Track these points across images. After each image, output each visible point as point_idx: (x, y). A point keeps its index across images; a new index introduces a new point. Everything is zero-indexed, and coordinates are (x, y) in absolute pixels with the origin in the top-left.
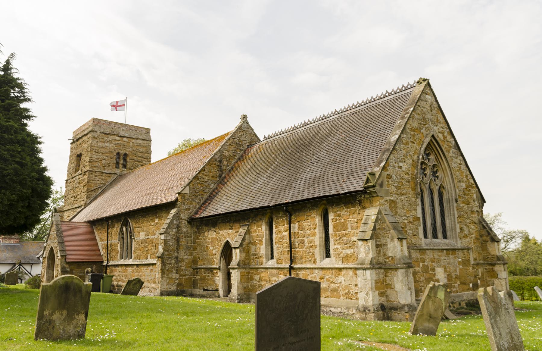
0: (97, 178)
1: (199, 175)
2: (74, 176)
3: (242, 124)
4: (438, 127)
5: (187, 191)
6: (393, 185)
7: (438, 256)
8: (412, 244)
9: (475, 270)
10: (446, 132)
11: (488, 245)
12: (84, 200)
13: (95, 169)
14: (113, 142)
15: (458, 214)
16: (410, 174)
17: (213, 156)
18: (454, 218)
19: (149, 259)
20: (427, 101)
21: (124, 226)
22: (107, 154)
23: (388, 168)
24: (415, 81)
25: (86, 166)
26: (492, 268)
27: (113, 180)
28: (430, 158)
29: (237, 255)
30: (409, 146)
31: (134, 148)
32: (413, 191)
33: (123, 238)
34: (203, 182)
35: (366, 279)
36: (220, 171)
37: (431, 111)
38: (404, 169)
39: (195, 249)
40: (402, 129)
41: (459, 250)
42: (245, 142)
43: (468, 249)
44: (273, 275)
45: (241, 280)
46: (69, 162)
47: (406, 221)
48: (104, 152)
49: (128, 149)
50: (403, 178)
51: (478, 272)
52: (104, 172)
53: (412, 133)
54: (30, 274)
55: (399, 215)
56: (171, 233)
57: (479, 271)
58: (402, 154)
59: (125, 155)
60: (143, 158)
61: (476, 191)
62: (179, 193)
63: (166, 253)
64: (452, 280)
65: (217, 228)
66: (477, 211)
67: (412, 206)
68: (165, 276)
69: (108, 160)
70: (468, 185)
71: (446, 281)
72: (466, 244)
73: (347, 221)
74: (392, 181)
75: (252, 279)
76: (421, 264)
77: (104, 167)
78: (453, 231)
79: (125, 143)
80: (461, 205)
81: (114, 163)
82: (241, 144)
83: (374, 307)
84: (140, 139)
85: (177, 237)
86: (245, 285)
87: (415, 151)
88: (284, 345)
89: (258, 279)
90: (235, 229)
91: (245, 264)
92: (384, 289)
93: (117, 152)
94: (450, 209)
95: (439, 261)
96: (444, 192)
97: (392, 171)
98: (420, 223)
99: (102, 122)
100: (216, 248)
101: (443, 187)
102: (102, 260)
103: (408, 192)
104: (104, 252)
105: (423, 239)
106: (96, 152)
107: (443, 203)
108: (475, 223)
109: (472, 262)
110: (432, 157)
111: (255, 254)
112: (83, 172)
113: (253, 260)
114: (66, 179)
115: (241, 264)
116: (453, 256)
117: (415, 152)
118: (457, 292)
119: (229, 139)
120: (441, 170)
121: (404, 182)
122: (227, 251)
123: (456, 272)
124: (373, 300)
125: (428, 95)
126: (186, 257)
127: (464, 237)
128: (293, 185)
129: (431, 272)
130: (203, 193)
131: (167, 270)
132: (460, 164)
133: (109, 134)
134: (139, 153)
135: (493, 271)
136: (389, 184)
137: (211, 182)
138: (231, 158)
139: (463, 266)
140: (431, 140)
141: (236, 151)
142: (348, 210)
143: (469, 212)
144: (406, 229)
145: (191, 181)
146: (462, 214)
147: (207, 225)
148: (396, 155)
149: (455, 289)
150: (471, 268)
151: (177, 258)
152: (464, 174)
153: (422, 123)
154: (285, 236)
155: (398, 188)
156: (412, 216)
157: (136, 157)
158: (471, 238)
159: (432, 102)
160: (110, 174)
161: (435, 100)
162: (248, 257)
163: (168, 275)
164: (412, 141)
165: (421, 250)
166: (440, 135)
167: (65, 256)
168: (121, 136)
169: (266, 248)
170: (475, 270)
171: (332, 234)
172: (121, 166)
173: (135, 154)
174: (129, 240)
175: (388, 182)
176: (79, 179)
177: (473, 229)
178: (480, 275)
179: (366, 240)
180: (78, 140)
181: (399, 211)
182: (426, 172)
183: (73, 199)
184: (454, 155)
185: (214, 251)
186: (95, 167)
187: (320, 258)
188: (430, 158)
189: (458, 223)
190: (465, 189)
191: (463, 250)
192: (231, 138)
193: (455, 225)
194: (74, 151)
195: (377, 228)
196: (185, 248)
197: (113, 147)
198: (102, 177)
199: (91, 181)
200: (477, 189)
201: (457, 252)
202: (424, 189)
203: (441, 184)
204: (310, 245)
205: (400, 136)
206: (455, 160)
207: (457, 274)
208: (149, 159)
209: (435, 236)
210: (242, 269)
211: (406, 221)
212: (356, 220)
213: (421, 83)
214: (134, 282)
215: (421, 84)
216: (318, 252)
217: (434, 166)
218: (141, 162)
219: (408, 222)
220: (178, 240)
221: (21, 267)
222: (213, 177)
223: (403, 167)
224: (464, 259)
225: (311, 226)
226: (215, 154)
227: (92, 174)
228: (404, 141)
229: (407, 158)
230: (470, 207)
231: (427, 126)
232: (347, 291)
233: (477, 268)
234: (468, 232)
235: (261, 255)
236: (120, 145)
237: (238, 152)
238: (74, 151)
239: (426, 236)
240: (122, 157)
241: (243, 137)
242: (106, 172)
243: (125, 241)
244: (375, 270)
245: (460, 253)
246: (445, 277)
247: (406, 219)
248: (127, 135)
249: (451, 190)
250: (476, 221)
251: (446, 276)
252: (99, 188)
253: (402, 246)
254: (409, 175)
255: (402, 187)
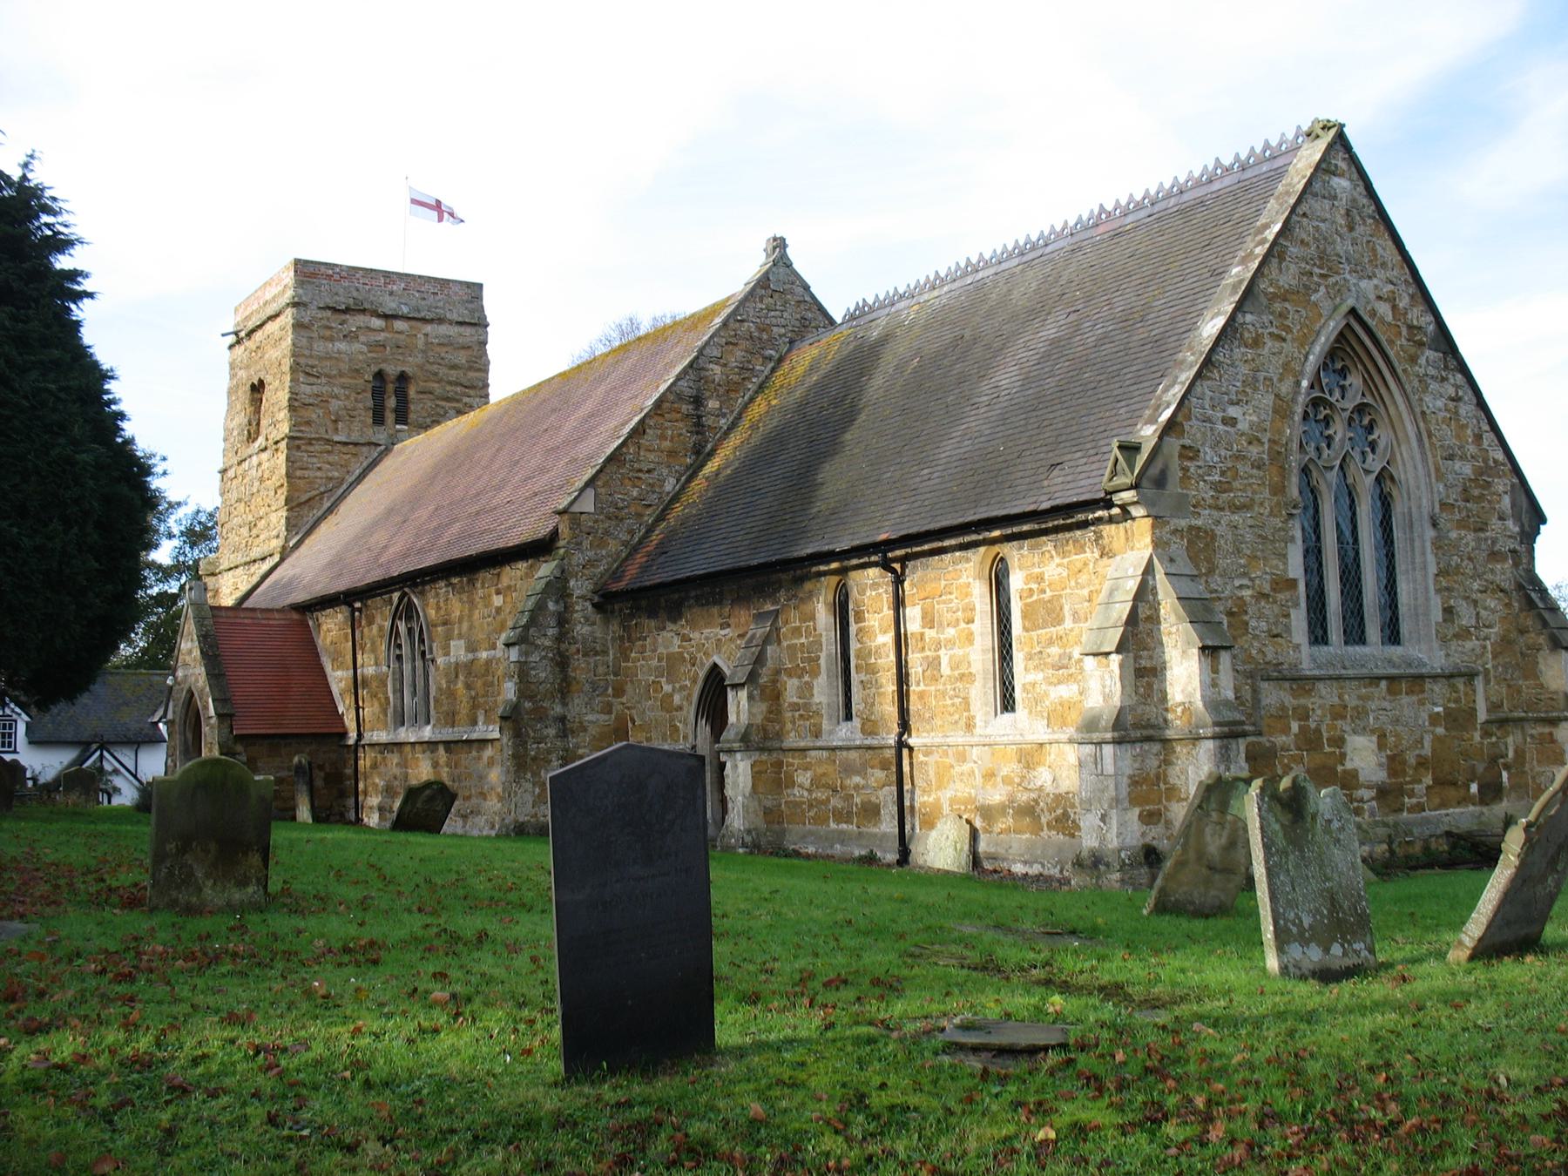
0: (315, 460)
1: (624, 450)
2: (245, 455)
3: (770, 268)
4: (1375, 281)
5: (587, 505)
6: (1205, 481)
7: (1360, 698)
8: (1267, 663)
9: (1494, 739)
10: (1405, 294)
11: (1540, 660)
12: (278, 536)
13: (310, 432)
14: (362, 338)
15: (1438, 564)
16: (1265, 440)
17: (672, 384)
18: (1425, 576)
19: (481, 726)
20: (1335, 198)
21: (401, 619)
22: (343, 380)
23: (1187, 428)
24: (1299, 127)
25: (277, 422)
26: (1551, 734)
27: (365, 464)
28: (1347, 383)
29: (739, 707)
30: (1266, 351)
31: (430, 353)
32: (1275, 494)
33: (399, 658)
34: (640, 471)
35: (1102, 774)
36: (697, 433)
37: (1351, 229)
38: (1243, 426)
39: (619, 692)
40: (1237, 298)
41: (1435, 677)
42: (782, 331)
43: (1470, 676)
44: (848, 769)
45: (754, 786)
46: (225, 408)
47: (1247, 593)
48: (334, 372)
49: (411, 359)
50: (1239, 457)
51: (1503, 748)
52: (336, 438)
53: (1278, 306)
54: (135, 776)
55: (1221, 576)
56: (538, 642)
57: (1506, 744)
58: (1240, 377)
59: (403, 378)
60: (462, 385)
61: (1513, 486)
62: (561, 513)
63: (528, 705)
64: (1404, 773)
65: (683, 622)
66: (1513, 552)
67: (1273, 544)
68: (529, 776)
69: (348, 397)
70: (1480, 467)
71: (1381, 776)
72: (1466, 658)
73: (1061, 596)
74: (1200, 467)
75: (792, 784)
76: (1295, 727)
77: (335, 421)
78: (1421, 617)
79: (402, 337)
80: (1453, 535)
81: (366, 409)
82: (765, 337)
83: (1123, 855)
84: (451, 323)
85: (560, 653)
86: (769, 804)
87: (1286, 366)
88: (617, 881)
89: (807, 784)
90: (737, 626)
91: (765, 738)
92: (1160, 802)
93: (375, 369)
94: (1413, 550)
95: (1360, 713)
96: (1395, 493)
97: (1199, 435)
98: (1298, 598)
99: (323, 269)
100: (683, 688)
101: (1392, 478)
102: (341, 730)
103: (1257, 501)
104: (347, 702)
105: (1305, 649)
106: (308, 374)
107: (1391, 530)
108: (1502, 591)
109: (1482, 716)
110: (1355, 380)
111: (798, 704)
112: (271, 442)
113: (793, 723)
114: (221, 466)
115: (755, 738)
116: (1415, 698)
117: (1285, 369)
118: (1420, 808)
119: (725, 324)
120: (1386, 420)
121: (1243, 468)
122: (714, 692)
123: (1423, 747)
124: (1119, 834)
125: (1342, 175)
126: (590, 717)
127: (1457, 636)
128: (911, 482)
129: (1327, 749)
130: (640, 509)
131: (534, 759)
132: (1456, 399)
133: (347, 310)
134: (445, 370)
135: (1553, 741)
136: (1189, 478)
137: (665, 472)
138: (731, 388)
139: (1446, 729)
140: (1348, 325)
141: (749, 362)
142: (1066, 561)
143: (1482, 556)
144: (1246, 618)
145: (600, 471)
146: (1453, 563)
147: (652, 613)
148: (1214, 383)
149: (1414, 800)
150: (1477, 736)
151: (562, 719)
152: (1469, 432)
153: (1317, 270)
154: (884, 645)
155: (1219, 488)
156: (1268, 577)
157: (436, 385)
158: (1485, 639)
159: (1354, 200)
160: (356, 444)
161: (1364, 193)
162: (775, 713)
163: (535, 774)
164: (1276, 331)
165: (1301, 682)
166: (1384, 309)
167: (231, 716)
168: (386, 317)
169: (830, 684)
170: (1494, 739)
171: (1019, 639)
172: (390, 417)
173: (436, 374)
174: (419, 663)
175: (1185, 470)
176: (260, 464)
177: (1494, 611)
178: (1511, 754)
179: (1108, 654)
180: (250, 334)
181: (1222, 563)
182: (1331, 432)
183: (245, 531)
184: (1431, 371)
185: (677, 699)
186: (308, 423)
187: (987, 713)
188: (1347, 383)
189: (1438, 591)
190: (1470, 480)
191: (1451, 676)
192: (732, 320)
193: (1427, 599)
194: (242, 374)
195: (1142, 615)
196: (587, 687)
197: (361, 353)
198: (331, 459)
199: (299, 473)
200: (1516, 480)
201: (1428, 686)
202: (1323, 487)
203: (1384, 468)
204: (956, 673)
205: (1232, 319)
206: (1434, 386)
207: (1423, 753)
208: (480, 389)
209: (1355, 634)
210: (758, 753)
211: (1247, 593)
212: (1085, 592)
213: (1318, 137)
214: (428, 792)
215: (1318, 142)
216: (983, 692)
217: (1361, 409)
218: (458, 401)
219: (1252, 596)
220: (562, 663)
221: (105, 753)
222: (672, 453)
223: (1240, 418)
224: (1453, 705)
225: (959, 613)
226: (678, 378)
227: (298, 447)
228: (1246, 335)
229: (1256, 389)
230: (1486, 540)
231: (1332, 280)
232: (1059, 812)
233: (1499, 734)
234: (1473, 622)
235: (814, 708)
236: (384, 346)
237: (758, 368)
238: (242, 374)
239: (1319, 634)
240: (390, 388)
241: (773, 313)
242: (342, 438)
243: (407, 667)
244: (1129, 746)
245: (1438, 689)
246: (1381, 765)
247: (1248, 587)
248: (405, 310)
249: (1418, 488)
250: (1504, 585)
251: (1384, 760)
252: (322, 493)
253: (1215, 670)
254: (1263, 443)
255: (1236, 484)
